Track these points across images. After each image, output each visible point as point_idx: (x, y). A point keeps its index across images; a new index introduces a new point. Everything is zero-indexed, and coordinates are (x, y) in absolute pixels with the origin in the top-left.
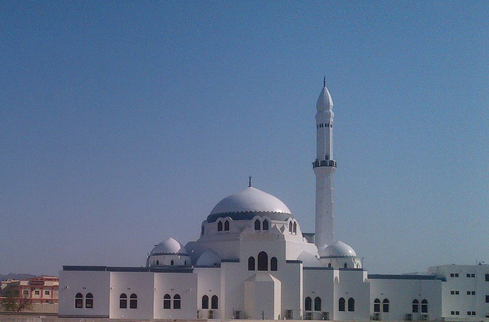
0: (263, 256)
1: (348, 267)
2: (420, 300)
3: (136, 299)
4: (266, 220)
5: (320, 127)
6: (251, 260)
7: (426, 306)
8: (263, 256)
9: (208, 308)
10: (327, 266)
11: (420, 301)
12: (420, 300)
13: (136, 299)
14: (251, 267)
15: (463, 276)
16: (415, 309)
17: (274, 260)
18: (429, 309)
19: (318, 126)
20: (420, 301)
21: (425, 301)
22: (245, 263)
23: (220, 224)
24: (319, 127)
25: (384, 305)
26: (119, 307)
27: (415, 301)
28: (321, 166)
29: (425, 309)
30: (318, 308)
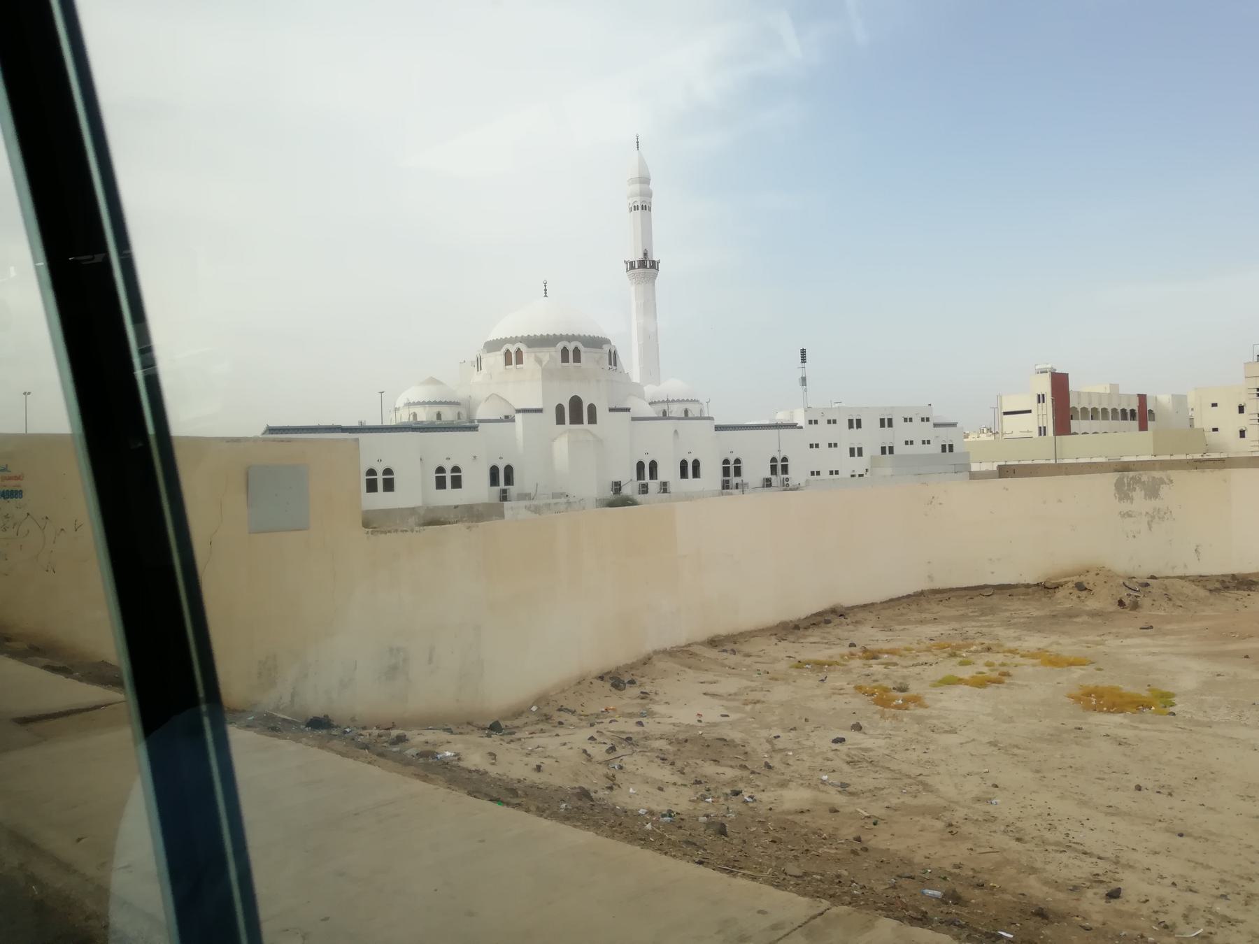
0: (576, 403)
1: (690, 415)
2: (380, 469)
3: (443, 475)
4: (576, 348)
5: (635, 210)
6: (560, 409)
7: (392, 480)
8: (576, 403)
9: (499, 485)
10: (661, 415)
11: (779, 459)
12: (380, 469)
13: (443, 475)
14: (560, 420)
15: (917, 420)
16: (773, 470)
17: (592, 409)
18: (790, 469)
19: (631, 209)
20: (779, 459)
21: (388, 471)
22: (551, 415)
23: (508, 353)
24: (633, 209)
25: (735, 467)
26: (680, 477)
27: (726, 461)
28: (639, 268)
29: (785, 469)
30: (653, 475)
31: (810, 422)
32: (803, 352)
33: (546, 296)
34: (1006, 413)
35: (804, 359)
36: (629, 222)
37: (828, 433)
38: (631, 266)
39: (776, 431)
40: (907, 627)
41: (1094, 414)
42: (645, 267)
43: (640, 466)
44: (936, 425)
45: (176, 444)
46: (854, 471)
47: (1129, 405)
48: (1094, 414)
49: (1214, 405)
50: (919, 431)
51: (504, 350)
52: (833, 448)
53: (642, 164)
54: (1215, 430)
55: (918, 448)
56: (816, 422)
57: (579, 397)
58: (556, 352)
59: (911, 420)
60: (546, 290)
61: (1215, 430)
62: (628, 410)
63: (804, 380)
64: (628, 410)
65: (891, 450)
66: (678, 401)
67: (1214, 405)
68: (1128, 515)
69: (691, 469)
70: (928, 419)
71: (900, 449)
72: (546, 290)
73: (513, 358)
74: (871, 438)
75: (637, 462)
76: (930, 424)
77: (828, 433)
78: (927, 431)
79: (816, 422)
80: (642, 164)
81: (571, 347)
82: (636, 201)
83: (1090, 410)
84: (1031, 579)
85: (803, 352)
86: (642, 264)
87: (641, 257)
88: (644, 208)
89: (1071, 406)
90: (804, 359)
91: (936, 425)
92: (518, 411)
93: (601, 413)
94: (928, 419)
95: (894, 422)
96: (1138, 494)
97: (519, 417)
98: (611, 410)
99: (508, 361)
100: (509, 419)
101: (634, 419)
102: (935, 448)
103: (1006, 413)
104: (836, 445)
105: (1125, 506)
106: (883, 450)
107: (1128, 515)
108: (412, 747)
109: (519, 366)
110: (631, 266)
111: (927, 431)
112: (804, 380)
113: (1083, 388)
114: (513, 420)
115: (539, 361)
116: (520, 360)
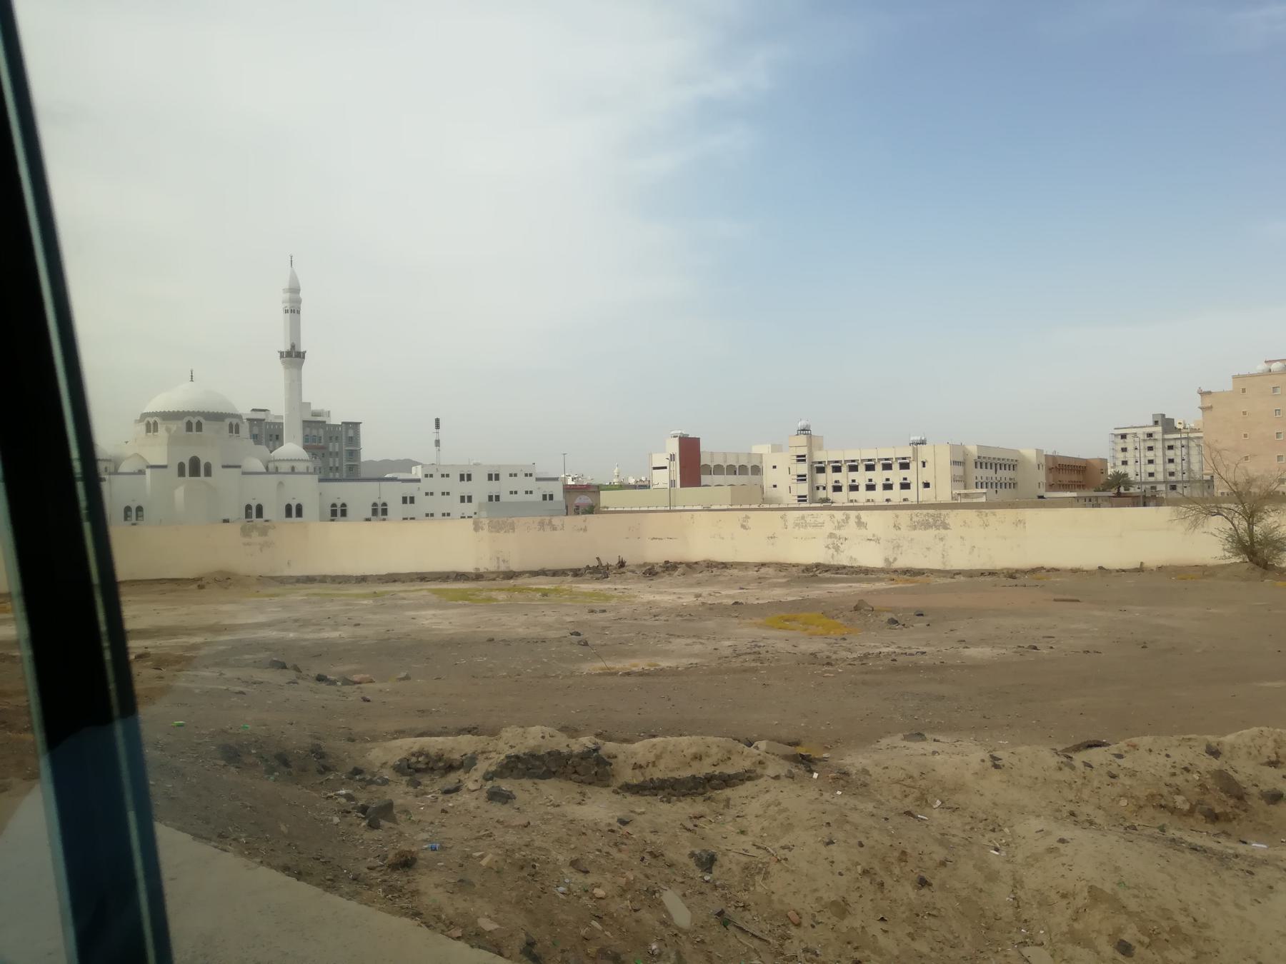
0: (195, 463)
1: (296, 471)
3: (548, 499)
7: (386, 509)
8: (195, 463)
10: (290, 471)
14: (181, 473)
22: (175, 470)
28: (286, 357)
31: (426, 476)
32: (437, 421)
33: (192, 381)
34: (655, 468)
35: (438, 426)
36: (280, 320)
37: (445, 485)
38: (282, 353)
39: (378, 483)
40: (176, 607)
41: (718, 470)
42: (291, 356)
43: (248, 507)
44: (538, 479)
45: (101, 466)
46: (463, 514)
47: (725, 462)
48: (718, 470)
49: (775, 467)
50: (522, 484)
51: (145, 422)
52: (514, 490)
53: (294, 278)
54: (775, 486)
55: (522, 497)
56: (431, 476)
57: (198, 459)
58: (181, 425)
59: (516, 475)
60: (192, 376)
61: (775, 486)
62: (239, 467)
63: (437, 443)
64: (239, 467)
65: (498, 498)
66: (287, 460)
67: (775, 467)
68: (248, 544)
69: (292, 511)
70: (531, 475)
71: (505, 497)
72: (192, 376)
73: (151, 428)
74: (479, 488)
75: (245, 506)
76: (533, 479)
77: (445, 485)
78: (530, 484)
79: (431, 476)
80: (294, 278)
81: (194, 421)
82: (286, 307)
83: (725, 467)
84: (190, 577)
85: (437, 421)
86: (289, 354)
87: (288, 348)
88: (293, 311)
89: (702, 464)
90: (438, 426)
91: (538, 479)
92: (148, 467)
93: (216, 470)
94: (531, 475)
95: (501, 477)
96: (255, 534)
97: (148, 471)
98: (224, 467)
99: (148, 430)
100: (141, 472)
101: (244, 473)
102: (537, 497)
103: (655, 468)
104: (448, 494)
105: (247, 540)
106: (490, 498)
107: (248, 544)
108: (516, 826)
109: (156, 434)
110: (282, 353)
111: (530, 484)
112: (437, 443)
113: (710, 451)
114: (144, 473)
115: (168, 430)
116: (156, 430)
